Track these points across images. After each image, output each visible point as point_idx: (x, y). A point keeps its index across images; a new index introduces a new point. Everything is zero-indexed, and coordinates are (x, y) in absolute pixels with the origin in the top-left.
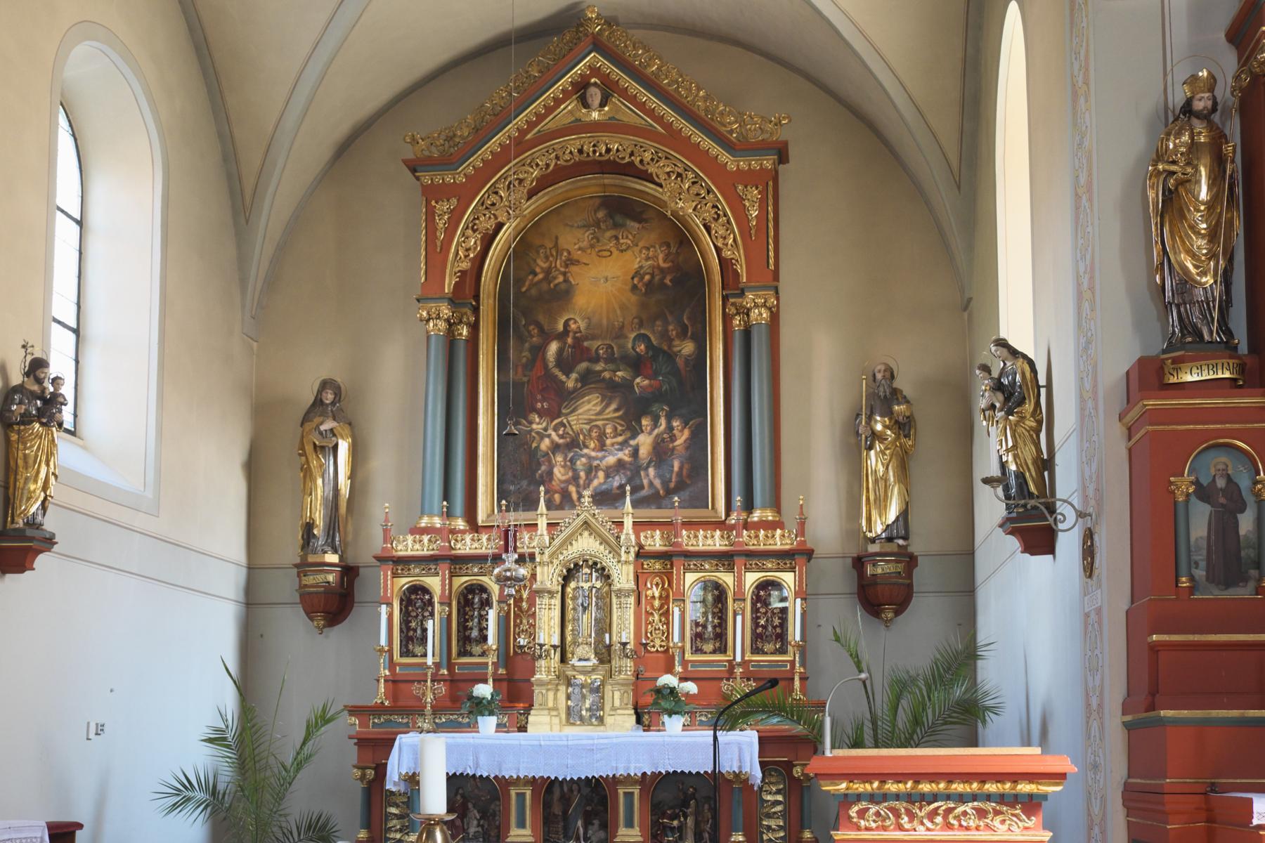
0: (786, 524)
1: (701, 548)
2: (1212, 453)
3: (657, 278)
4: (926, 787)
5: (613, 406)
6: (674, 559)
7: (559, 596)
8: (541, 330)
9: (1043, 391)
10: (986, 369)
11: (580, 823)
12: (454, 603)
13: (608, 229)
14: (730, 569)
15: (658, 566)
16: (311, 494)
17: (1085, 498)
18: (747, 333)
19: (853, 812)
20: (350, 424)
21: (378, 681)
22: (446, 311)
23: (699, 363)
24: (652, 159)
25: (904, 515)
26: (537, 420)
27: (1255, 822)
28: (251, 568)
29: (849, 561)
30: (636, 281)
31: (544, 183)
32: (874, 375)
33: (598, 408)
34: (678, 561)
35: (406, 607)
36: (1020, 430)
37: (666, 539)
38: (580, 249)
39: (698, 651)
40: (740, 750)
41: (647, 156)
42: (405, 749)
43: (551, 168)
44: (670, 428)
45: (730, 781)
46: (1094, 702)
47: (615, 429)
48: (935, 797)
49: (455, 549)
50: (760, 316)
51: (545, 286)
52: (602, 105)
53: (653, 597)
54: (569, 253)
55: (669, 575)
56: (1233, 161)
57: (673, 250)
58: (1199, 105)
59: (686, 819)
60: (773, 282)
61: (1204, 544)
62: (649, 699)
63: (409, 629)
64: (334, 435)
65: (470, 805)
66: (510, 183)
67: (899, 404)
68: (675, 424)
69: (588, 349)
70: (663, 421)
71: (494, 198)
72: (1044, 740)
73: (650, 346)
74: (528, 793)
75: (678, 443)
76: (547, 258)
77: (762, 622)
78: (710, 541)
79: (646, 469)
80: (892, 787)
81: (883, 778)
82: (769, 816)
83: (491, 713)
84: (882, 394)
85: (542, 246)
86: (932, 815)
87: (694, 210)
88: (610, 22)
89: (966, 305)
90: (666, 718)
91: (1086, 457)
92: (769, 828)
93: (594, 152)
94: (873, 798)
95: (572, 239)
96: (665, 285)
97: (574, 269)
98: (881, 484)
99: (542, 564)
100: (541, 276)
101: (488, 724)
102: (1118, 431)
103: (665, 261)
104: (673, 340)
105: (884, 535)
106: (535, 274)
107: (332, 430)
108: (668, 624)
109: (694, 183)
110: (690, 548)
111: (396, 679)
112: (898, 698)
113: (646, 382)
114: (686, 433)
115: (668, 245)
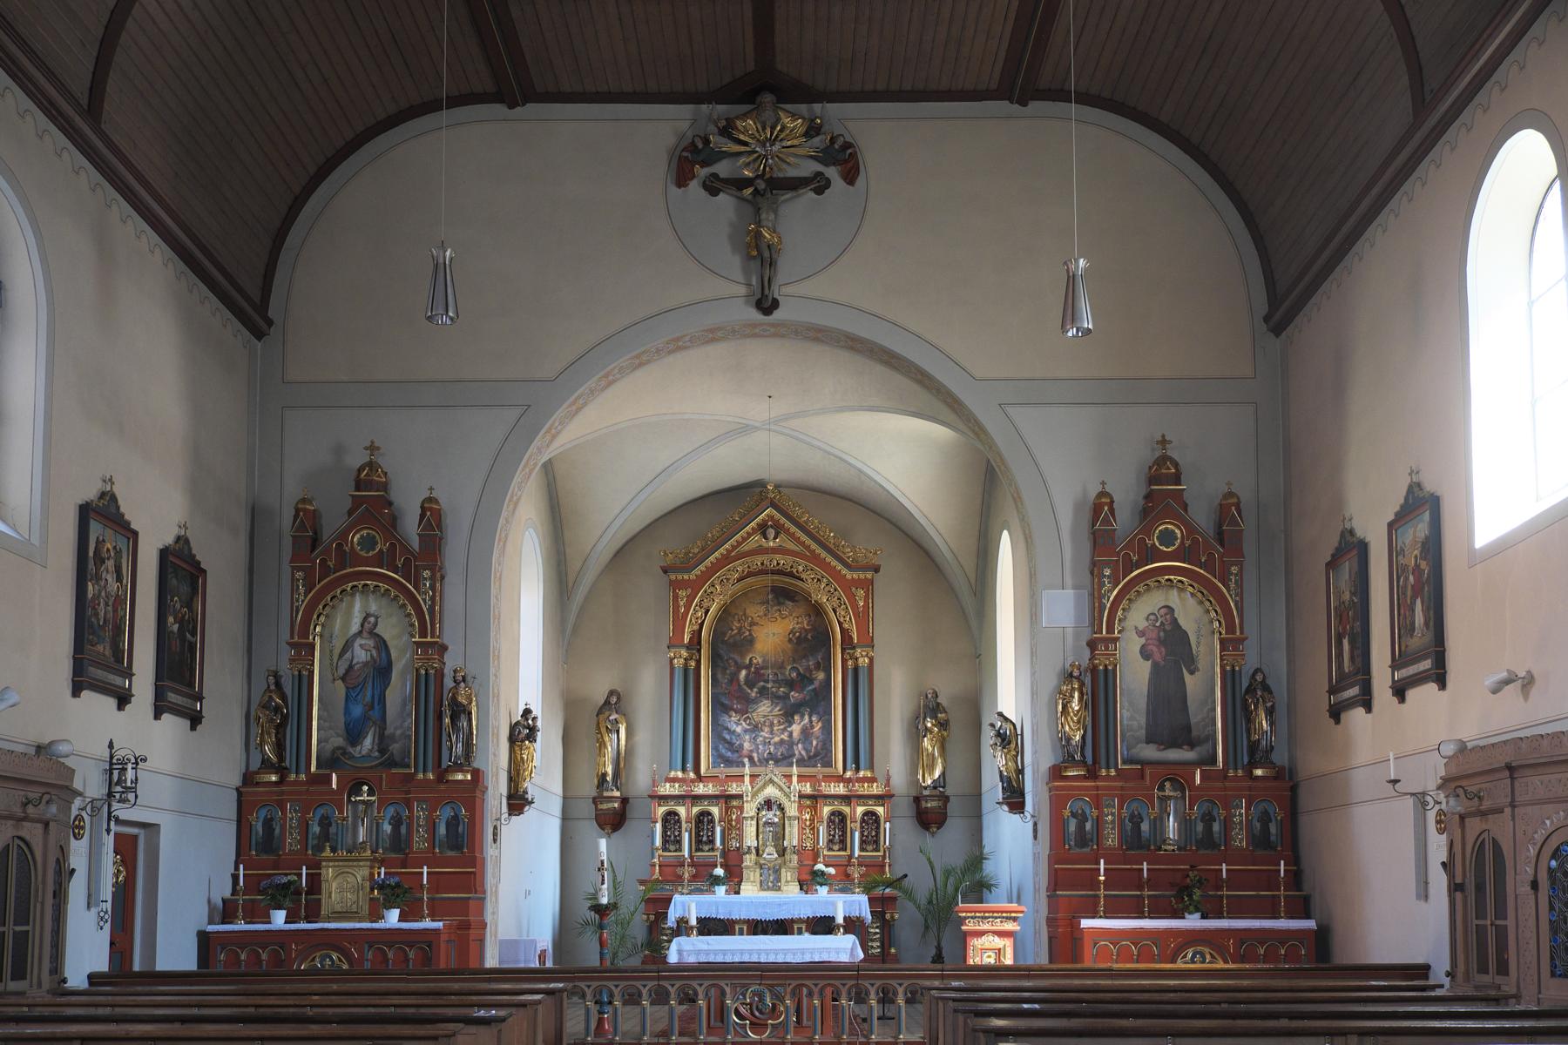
0: (879, 780)
3: (803, 635)
4: (987, 915)
5: (778, 708)
8: (736, 663)
9: (1019, 737)
10: (993, 725)
12: (693, 822)
13: (775, 605)
14: (849, 804)
15: (808, 803)
16: (605, 756)
18: (856, 670)
19: (967, 921)
20: (624, 715)
22: (685, 653)
23: (827, 684)
25: (943, 774)
27: (1082, 926)
28: (565, 798)
30: (791, 636)
32: (927, 695)
33: (769, 710)
35: (666, 822)
36: (1008, 756)
39: (830, 849)
40: (860, 905)
41: (801, 568)
42: (678, 904)
44: (811, 721)
45: (853, 921)
47: (779, 721)
48: (989, 917)
51: (738, 638)
52: (775, 538)
57: (812, 618)
58: (1075, 674)
60: (870, 643)
62: (808, 877)
63: (666, 835)
64: (617, 722)
66: (722, 580)
68: (814, 719)
69: (764, 675)
70: (807, 717)
71: (712, 589)
72: (1019, 901)
73: (799, 674)
74: (745, 928)
77: (865, 834)
78: (837, 789)
79: (797, 745)
80: (978, 914)
81: (975, 912)
82: (872, 941)
83: (723, 884)
84: (931, 707)
85: (736, 614)
86: (988, 922)
90: (818, 887)
91: (1035, 796)
92: (872, 947)
94: (972, 918)
95: (755, 611)
97: (755, 628)
99: (747, 801)
100: (736, 631)
101: (721, 890)
102: (1046, 788)
103: (807, 625)
104: (811, 671)
106: (733, 630)
109: (827, 585)
112: (947, 878)
113: (797, 694)
114: (820, 724)
115: (810, 616)
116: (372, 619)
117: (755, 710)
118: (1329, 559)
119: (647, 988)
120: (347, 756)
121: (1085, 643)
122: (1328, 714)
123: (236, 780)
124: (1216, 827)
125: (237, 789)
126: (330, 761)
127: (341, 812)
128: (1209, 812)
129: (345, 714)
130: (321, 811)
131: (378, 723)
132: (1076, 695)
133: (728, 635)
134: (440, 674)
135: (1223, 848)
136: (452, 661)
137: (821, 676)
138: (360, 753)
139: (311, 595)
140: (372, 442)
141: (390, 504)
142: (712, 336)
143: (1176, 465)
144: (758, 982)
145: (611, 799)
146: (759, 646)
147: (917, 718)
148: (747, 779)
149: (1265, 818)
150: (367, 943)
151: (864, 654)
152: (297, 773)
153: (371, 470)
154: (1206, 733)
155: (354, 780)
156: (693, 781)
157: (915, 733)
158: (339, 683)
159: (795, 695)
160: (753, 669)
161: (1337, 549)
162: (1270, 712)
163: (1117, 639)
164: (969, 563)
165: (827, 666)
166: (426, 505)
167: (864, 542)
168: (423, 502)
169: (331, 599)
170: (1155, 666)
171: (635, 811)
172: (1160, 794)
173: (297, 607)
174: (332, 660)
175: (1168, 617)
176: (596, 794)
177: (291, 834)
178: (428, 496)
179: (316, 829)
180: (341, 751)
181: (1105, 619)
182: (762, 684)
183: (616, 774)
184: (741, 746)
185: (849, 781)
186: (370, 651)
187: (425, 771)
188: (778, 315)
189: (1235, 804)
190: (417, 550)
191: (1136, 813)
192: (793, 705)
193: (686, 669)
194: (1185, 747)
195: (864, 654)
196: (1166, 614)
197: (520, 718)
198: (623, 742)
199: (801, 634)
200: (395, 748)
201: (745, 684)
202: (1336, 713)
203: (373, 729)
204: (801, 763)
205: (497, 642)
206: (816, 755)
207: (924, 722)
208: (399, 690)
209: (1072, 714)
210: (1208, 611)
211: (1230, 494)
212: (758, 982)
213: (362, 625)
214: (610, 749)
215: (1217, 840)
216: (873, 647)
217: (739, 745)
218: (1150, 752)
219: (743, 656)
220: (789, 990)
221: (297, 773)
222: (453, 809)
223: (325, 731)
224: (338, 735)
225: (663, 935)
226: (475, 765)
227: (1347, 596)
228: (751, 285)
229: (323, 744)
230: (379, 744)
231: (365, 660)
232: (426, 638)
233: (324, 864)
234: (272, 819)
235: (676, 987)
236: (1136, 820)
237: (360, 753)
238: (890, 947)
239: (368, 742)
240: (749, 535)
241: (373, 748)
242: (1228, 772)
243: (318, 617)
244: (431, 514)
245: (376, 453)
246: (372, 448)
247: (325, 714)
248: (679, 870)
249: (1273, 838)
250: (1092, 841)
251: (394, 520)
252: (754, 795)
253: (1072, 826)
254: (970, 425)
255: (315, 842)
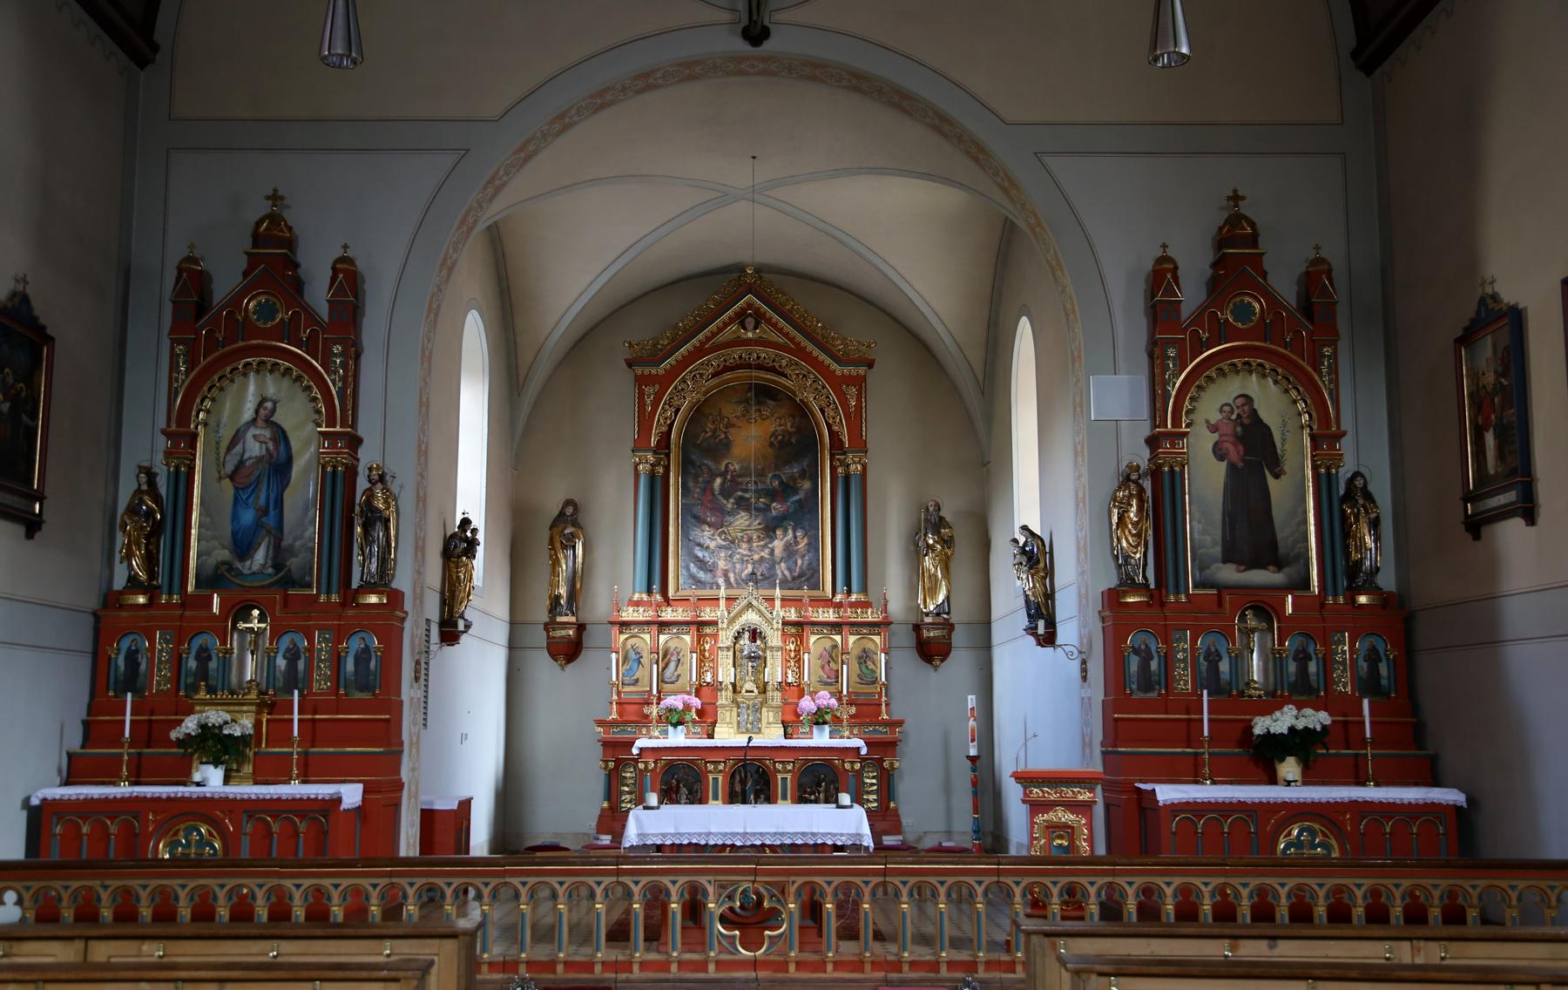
0: (873, 605)
1: (821, 619)
2: (1140, 634)
5: (758, 522)
6: (805, 626)
7: (732, 650)
8: (710, 469)
11: (752, 797)
14: (840, 633)
16: (558, 576)
17: (1081, 643)
18: (847, 478)
21: (611, 703)
22: (651, 458)
24: (787, 365)
25: (948, 598)
26: (707, 529)
28: (513, 623)
29: (911, 627)
30: (772, 439)
31: (715, 375)
33: (748, 523)
34: (807, 629)
37: (798, 612)
38: (735, 417)
43: (721, 367)
44: (795, 537)
46: (1087, 739)
47: (759, 537)
49: (660, 617)
50: (855, 468)
52: (756, 328)
53: (790, 650)
54: (728, 419)
55: (801, 637)
56: (1148, 502)
59: (819, 794)
60: (861, 446)
61: (1136, 674)
64: (573, 536)
65: (681, 785)
66: (695, 375)
67: (944, 529)
68: (798, 534)
70: (790, 532)
71: (683, 386)
73: (782, 483)
74: (720, 778)
75: (800, 546)
76: (714, 422)
78: (826, 615)
84: (933, 521)
85: (710, 414)
87: (815, 399)
88: (759, 270)
89: (985, 464)
92: (868, 801)
93: (750, 358)
95: (731, 410)
96: (792, 443)
97: (732, 430)
98: (933, 579)
99: (722, 629)
100: (710, 434)
103: (791, 427)
104: (796, 479)
105: (935, 611)
106: (706, 433)
107: (571, 533)
108: (799, 668)
109: (814, 381)
110: (815, 619)
111: (622, 701)
113: (779, 506)
114: (806, 541)
115: (794, 416)
116: (269, 405)
117: (730, 524)
118: (1459, 333)
119: (602, 886)
120: (233, 573)
121: (1143, 440)
122: (1463, 527)
123: (92, 602)
124: (1312, 667)
125: (94, 614)
126: (212, 579)
127: (224, 642)
128: (1303, 648)
129: (233, 521)
130: (197, 642)
131: (273, 532)
132: (1134, 502)
133: (701, 438)
134: (352, 472)
135: (1322, 694)
136: (367, 456)
137: (807, 485)
138: (250, 569)
139: (194, 373)
140: (275, 190)
141: (296, 266)
142: (690, 71)
143: (1253, 225)
144: (752, 878)
145: (565, 625)
146: (736, 451)
147: (917, 534)
148: (722, 603)
149: (1373, 657)
150: (245, 812)
151: (857, 460)
152: (170, 594)
153: (271, 223)
154: (1296, 551)
155: (237, 604)
156: (659, 605)
157: (915, 552)
158: (227, 483)
159: (777, 508)
160: (729, 477)
161: (1473, 321)
162: (1375, 525)
163: (1185, 434)
164: (976, 355)
165: (813, 475)
166: (338, 266)
167: (856, 331)
168: (336, 262)
169: (220, 379)
170: (1232, 468)
171: (591, 638)
172: (1242, 625)
173: (176, 389)
174: (218, 454)
175: (1246, 408)
176: (548, 620)
177: (160, 670)
178: (341, 255)
179: (192, 664)
180: (226, 567)
181: (1170, 409)
182: (740, 493)
183: (573, 595)
184: (715, 565)
185: (839, 605)
186: (265, 443)
187: (329, 593)
188: (768, 46)
189: (1336, 638)
190: (326, 319)
191: (1213, 649)
192: (774, 518)
193: (652, 477)
194: (1271, 568)
195: (857, 460)
196: (1243, 405)
197: (457, 530)
198: (580, 559)
199: (783, 437)
200: (294, 563)
201: (720, 494)
202: (1476, 527)
203: (267, 539)
204: (785, 584)
205: (424, 435)
206: (800, 576)
207: (925, 539)
208: (303, 488)
209: (1130, 526)
210: (1295, 402)
211: (1319, 261)
212: (752, 878)
213: (257, 412)
214: (564, 568)
215: (1314, 684)
216: (867, 451)
217: (713, 563)
218: (1229, 574)
219: (717, 460)
220: (793, 889)
221: (170, 594)
222: (364, 639)
223: (208, 542)
224: (224, 547)
225: (624, 786)
226: (394, 585)
227: (1490, 379)
228: (736, 11)
229: (204, 558)
230: (275, 558)
231: (258, 455)
232: (335, 427)
233: (198, 708)
234: (137, 651)
235: (641, 885)
236: (1213, 658)
237: (250, 569)
238: (889, 801)
239: (260, 556)
240: (726, 325)
241: (266, 562)
242: (1325, 599)
243: (202, 401)
244: (347, 279)
245: (278, 203)
246: (275, 198)
247: (208, 519)
248: (646, 710)
249: (1384, 682)
250: (1159, 684)
251: (298, 286)
252: (732, 621)
253: (1134, 663)
254: (999, 180)
255: (190, 680)
